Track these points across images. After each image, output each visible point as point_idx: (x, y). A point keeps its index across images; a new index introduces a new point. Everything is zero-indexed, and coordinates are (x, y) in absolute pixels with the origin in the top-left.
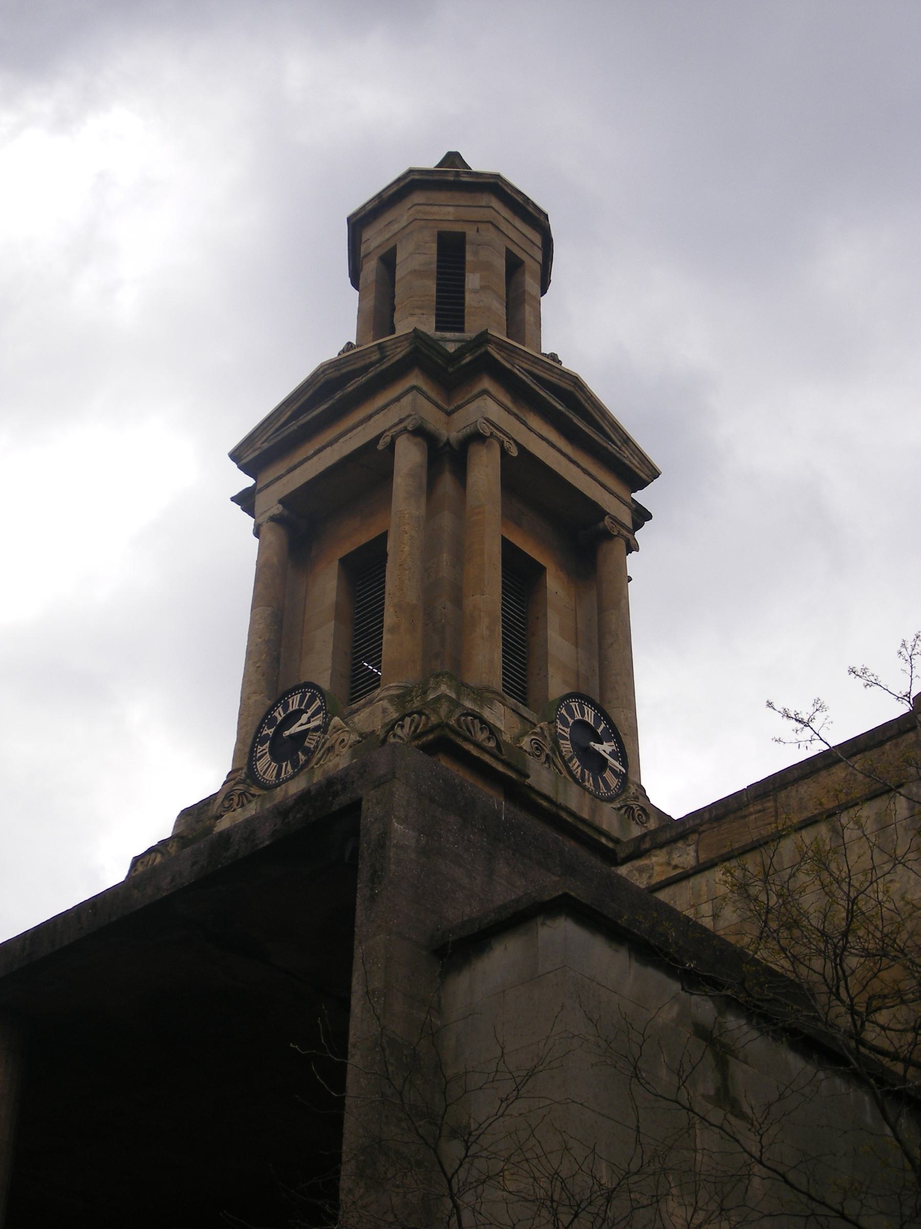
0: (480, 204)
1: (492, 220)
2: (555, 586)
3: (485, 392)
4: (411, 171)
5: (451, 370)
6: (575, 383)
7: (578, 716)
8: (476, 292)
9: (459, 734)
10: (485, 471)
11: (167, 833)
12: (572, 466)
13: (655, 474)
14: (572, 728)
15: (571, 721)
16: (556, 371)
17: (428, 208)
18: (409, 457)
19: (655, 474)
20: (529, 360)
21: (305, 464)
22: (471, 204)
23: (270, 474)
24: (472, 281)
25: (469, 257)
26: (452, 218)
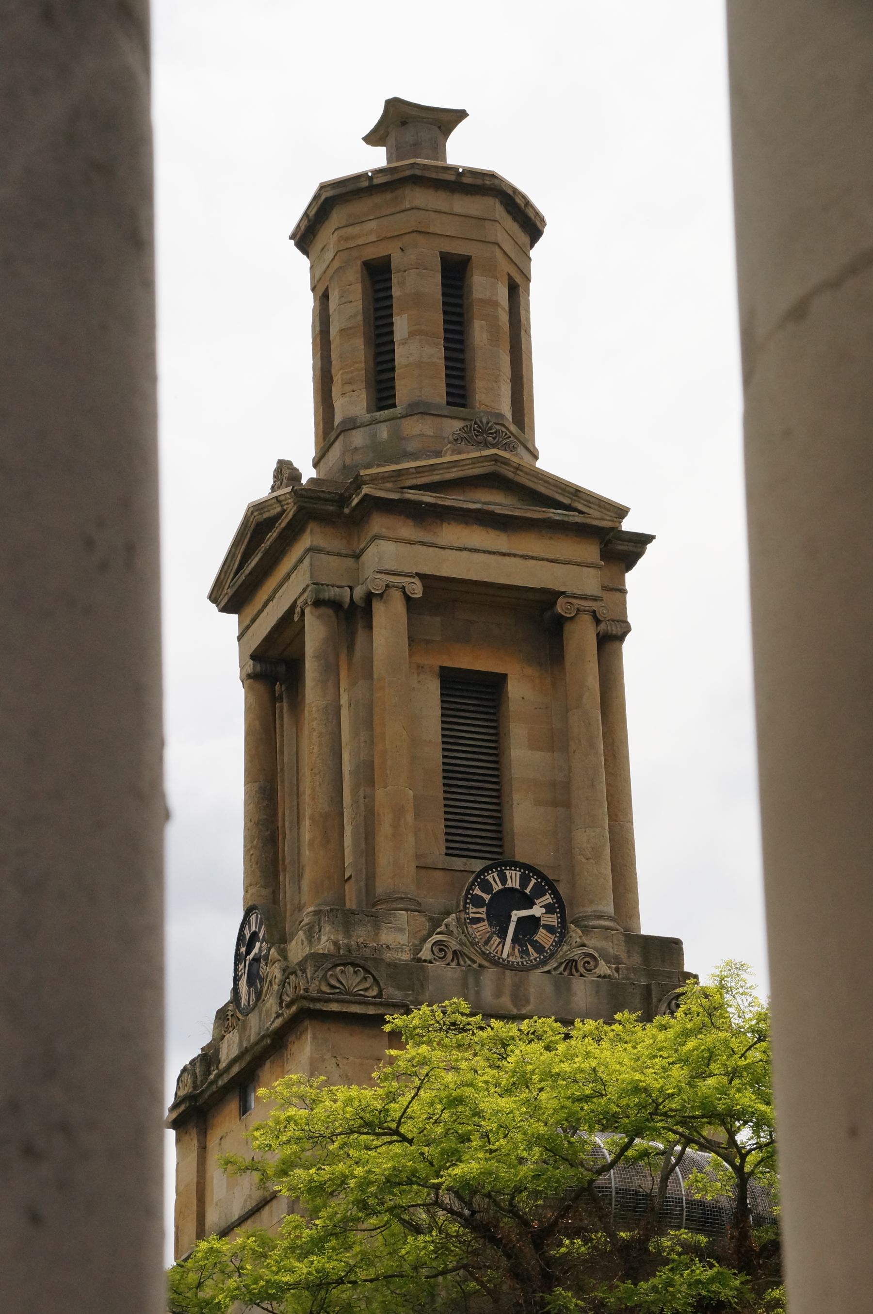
0: (403, 208)
1: (415, 229)
2: (521, 691)
3: (375, 537)
4: (323, 187)
5: (347, 511)
6: (496, 461)
7: (497, 887)
8: (404, 343)
9: (318, 1000)
10: (388, 626)
11: (648, 546)
12: (507, 559)
13: (629, 509)
14: (490, 906)
15: (487, 897)
16: (465, 462)
17: (350, 229)
18: (315, 633)
19: (629, 509)
20: (424, 472)
21: (261, 616)
22: (393, 210)
23: (251, 610)
24: (401, 326)
25: (396, 292)
26: (375, 239)
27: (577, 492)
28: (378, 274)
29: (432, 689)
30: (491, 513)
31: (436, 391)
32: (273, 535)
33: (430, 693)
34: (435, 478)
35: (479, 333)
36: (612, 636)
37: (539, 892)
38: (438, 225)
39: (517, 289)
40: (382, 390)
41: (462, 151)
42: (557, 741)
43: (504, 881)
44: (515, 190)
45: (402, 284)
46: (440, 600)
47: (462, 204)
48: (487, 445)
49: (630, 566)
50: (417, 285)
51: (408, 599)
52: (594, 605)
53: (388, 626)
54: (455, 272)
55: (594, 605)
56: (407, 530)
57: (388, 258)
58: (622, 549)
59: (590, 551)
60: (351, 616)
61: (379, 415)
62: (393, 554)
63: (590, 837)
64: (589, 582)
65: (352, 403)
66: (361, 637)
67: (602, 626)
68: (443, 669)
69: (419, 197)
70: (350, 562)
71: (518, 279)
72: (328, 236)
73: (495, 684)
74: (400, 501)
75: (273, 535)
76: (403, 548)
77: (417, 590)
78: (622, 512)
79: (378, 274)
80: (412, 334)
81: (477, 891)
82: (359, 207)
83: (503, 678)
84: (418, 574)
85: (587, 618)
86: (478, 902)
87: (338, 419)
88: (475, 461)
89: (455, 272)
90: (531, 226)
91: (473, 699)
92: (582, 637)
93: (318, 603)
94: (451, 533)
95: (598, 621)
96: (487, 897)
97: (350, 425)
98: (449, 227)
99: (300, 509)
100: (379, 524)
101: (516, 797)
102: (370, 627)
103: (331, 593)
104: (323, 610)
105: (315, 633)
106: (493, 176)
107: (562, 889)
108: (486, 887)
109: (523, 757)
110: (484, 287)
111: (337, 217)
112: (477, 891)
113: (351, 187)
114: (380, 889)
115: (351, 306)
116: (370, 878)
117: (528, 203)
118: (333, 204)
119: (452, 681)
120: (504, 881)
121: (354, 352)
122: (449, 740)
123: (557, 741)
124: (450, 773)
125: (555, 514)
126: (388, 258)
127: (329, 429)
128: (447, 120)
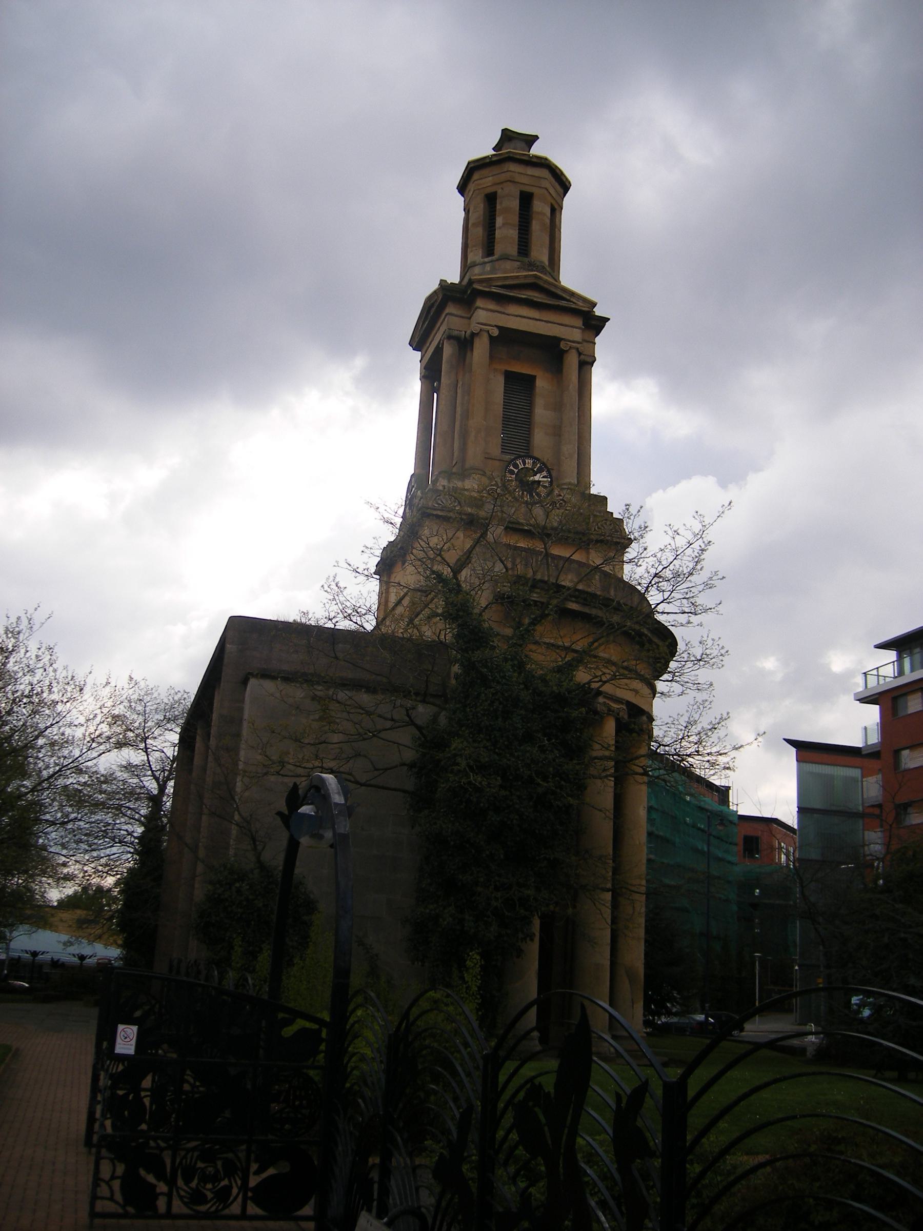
2: (542, 383)
8: (500, 228)
10: (481, 348)
12: (538, 322)
14: (517, 475)
15: (516, 471)
18: (448, 350)
24: (499, 221)
25: (498, 207)
27: (573, 294)
28: (491, 199)
29: (501, 380)
30: (532, 300)
31: (513, 250)
32: (433, 310)
33: (499, 384)
34: (507, 282)
35: (535, 226)
36: (587, 363)
37: (540, 471)
38: (518, 179)
39: (556, 210)
40: (489, 250)
41: (536, 150)
42: (558, 407)
43: (524, 464)
44: (556, 167)
45: (501, 203)
46: (507, 340)
47: (531, 171)
48: (532, 271)
49: (597, 334)
50: (509, 204)
51: (491, 337)
52: (578, 346)
53: (481, 348)
54: (526, 199)
55: (578, 346)
56: (492, 306)
57: (495, 193)
58: (595, 325)
59: (579, 322)
60: (465, 344)
61: (486, 260)
62: (486, 316)
63: (569, 448)
64: (576, 335)
65: (476, 256)
66: (469, 354)
67: (582, 357)
68: (506, 371)
69: (512, 167)
70: (466, 321)
71: (556, 206)
72: (471, 187)
73: (531, 379)
74: (489, 292)
75: (433, 310)
76: (490, 314)
77: (495, 332)
78: (594, 305)
79: (491, 199)
80: (504, 224)
81: (512, 468)
82: (485, 172)
83: (533, 378)
84: (496, 326)
85: (574, 351)
86: (512, 472)
87: (469, 261)
88: (526, 276)
89: (526, 199)
90: (564, 185)
91: (520, 387)
92: (572, 361)
93: (450, 337)
94: (513, 309)
95: (580, 354)
96: (516, 471)
97: (474, 265)
98: (525, 180)
99: (444, 295)
100: (479, 303)
101: (536, 431)
102: (472, 350)
103: (455, 333)
104: (452, 341)
105: (448, 350)
106: (546, 159)
107: (554, 474)
108: (516, 466)
109: (542, 413)
110: (540, 207)
111: (476, 176)
112: (512, 468)
113: (481, 162)
114: (467, 466)
115: (479, 212)
116: (464, 460)
117: (562, 173)
118: (474, 169)
119: (510, 377)
120: (524, 464)
121: (478, 232)
122: (506, 404)
123: (558, 407)
124: (506, 419)
125: (563, 303)
126: (495, 193)
127: (466, 266)
128: (531, 140)
